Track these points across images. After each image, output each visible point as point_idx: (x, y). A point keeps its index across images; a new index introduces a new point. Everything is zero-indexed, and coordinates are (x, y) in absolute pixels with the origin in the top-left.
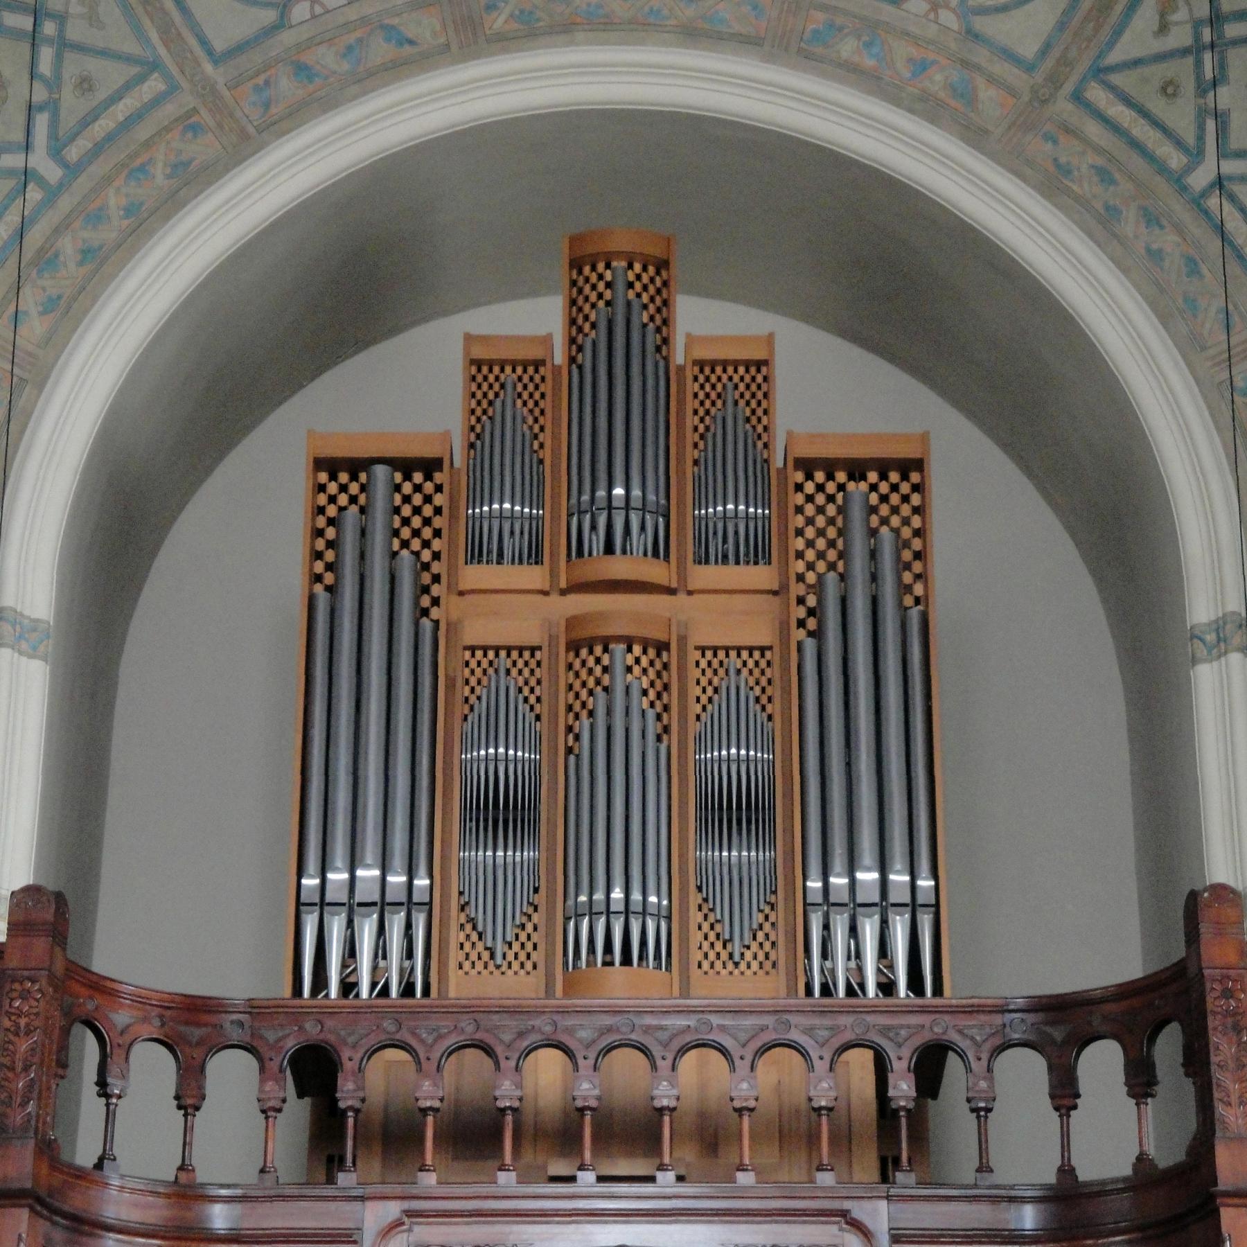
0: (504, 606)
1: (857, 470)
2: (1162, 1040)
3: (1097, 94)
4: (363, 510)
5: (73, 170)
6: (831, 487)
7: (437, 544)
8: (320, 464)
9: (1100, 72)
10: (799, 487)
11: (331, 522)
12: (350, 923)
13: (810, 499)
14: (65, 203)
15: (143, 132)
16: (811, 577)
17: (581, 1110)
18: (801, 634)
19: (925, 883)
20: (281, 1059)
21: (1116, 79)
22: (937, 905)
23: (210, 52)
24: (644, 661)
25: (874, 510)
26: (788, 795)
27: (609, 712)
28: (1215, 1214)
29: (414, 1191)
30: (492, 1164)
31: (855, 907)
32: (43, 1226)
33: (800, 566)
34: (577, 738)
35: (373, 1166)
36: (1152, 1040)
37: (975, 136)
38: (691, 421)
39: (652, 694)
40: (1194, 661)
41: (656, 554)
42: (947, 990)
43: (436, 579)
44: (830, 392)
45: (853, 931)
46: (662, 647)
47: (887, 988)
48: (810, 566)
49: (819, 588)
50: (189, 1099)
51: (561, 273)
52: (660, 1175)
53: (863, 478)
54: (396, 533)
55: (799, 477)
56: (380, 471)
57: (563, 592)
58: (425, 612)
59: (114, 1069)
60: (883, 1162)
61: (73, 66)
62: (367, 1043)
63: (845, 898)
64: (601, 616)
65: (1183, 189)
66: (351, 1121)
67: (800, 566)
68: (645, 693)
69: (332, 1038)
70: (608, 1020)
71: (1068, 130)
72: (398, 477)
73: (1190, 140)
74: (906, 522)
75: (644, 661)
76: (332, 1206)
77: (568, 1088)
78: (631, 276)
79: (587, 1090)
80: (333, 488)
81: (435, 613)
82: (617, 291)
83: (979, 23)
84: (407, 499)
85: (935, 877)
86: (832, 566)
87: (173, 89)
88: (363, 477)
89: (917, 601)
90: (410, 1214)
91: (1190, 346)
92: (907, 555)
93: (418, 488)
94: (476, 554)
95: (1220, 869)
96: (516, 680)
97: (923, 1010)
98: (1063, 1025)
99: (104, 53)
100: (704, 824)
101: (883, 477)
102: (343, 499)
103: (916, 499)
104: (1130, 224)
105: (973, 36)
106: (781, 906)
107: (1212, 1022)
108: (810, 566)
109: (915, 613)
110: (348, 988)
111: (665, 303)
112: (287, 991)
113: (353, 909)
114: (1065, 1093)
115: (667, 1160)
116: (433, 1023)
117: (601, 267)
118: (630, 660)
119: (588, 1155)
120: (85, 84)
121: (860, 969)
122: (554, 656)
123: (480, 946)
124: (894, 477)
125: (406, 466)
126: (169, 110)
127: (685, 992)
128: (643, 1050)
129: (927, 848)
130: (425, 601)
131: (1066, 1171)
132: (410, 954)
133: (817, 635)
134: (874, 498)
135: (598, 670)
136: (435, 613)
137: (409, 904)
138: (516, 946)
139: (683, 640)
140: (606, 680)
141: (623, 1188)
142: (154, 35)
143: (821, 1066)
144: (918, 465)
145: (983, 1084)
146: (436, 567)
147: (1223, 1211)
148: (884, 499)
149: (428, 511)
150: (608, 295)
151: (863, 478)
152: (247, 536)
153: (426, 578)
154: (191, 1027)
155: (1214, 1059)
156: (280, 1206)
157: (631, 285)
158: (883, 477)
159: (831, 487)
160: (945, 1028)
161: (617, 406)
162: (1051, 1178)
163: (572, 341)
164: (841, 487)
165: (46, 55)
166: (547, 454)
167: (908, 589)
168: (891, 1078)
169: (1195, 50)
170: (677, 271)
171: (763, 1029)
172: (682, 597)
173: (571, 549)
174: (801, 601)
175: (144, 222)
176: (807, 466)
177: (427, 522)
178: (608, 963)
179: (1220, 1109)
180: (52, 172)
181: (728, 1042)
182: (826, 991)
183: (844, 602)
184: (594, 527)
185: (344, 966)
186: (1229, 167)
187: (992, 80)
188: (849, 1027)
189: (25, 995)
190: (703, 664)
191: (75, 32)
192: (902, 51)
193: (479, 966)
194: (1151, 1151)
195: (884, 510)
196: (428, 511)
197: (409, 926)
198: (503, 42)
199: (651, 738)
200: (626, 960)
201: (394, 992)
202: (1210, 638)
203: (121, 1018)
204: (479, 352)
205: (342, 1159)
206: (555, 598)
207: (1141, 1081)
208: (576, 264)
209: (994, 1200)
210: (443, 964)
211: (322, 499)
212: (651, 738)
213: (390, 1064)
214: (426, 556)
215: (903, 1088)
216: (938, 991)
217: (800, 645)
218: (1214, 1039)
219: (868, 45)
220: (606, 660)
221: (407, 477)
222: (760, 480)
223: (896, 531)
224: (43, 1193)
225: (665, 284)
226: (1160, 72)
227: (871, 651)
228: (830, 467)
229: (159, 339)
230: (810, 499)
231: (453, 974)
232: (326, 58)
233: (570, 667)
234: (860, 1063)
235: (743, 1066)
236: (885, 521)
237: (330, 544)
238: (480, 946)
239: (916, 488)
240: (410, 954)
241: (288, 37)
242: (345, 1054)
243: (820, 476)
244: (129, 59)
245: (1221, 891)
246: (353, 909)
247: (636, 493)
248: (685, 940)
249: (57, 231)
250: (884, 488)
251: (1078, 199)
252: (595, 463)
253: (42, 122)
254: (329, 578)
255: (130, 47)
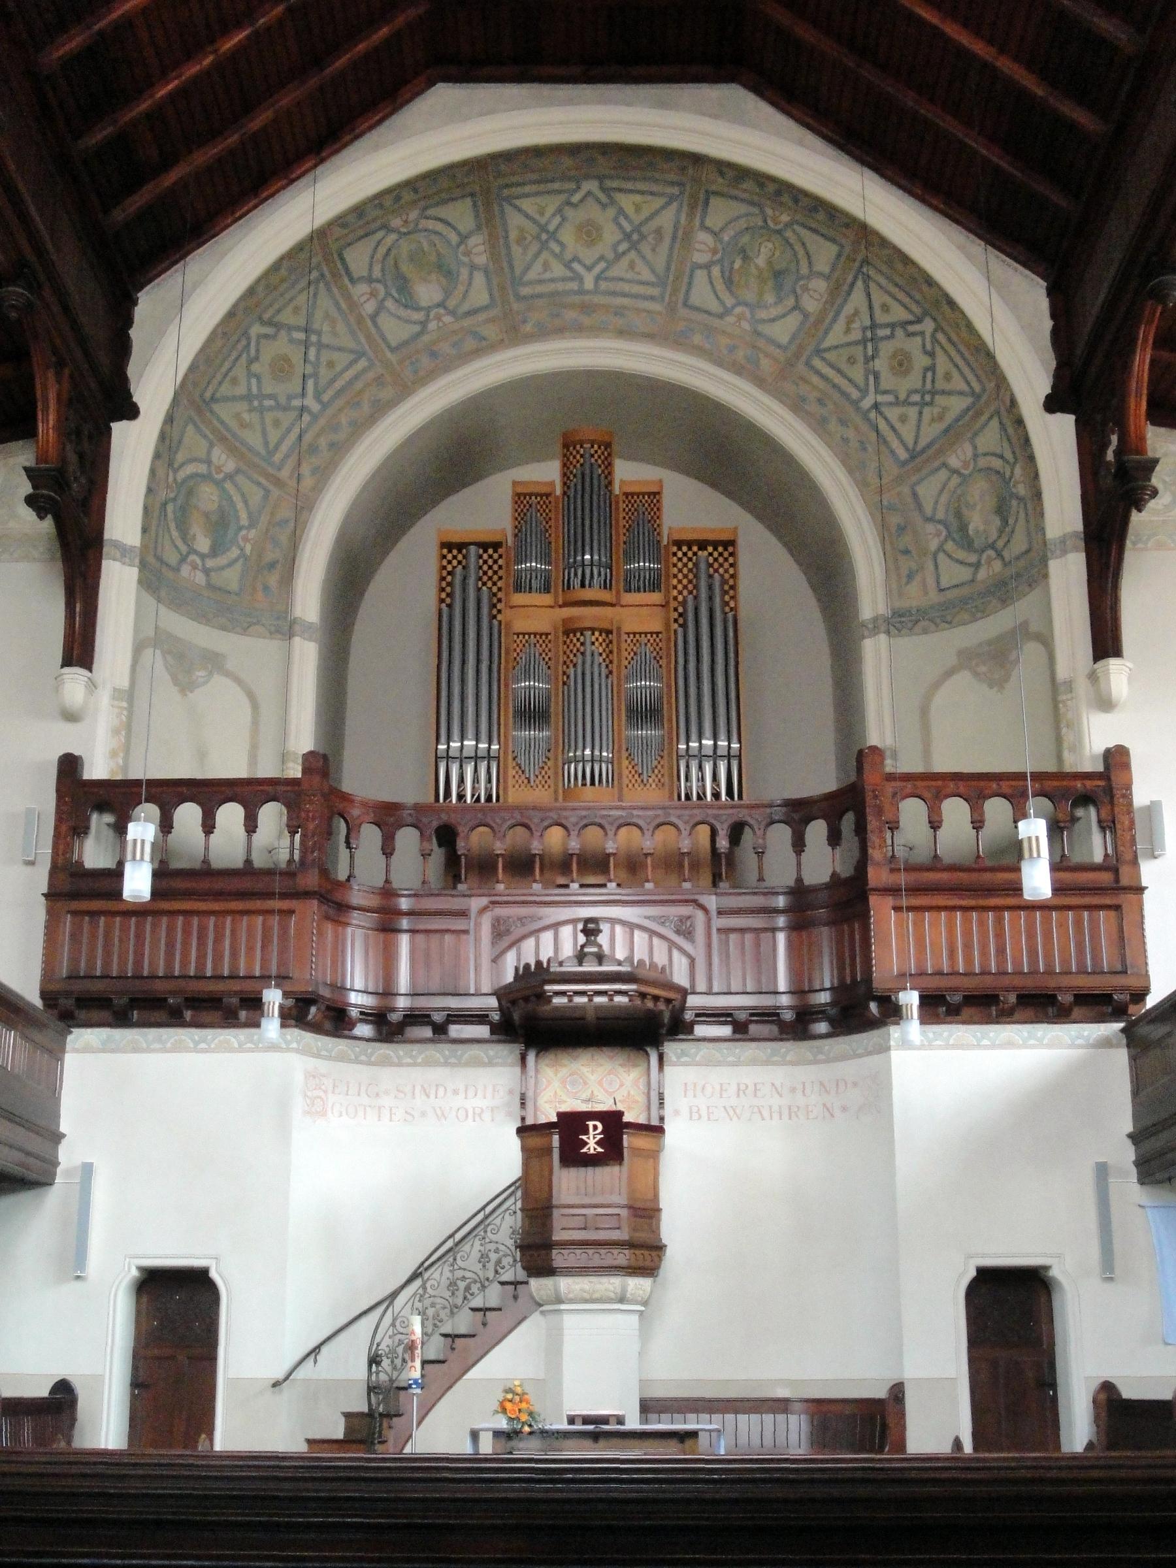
0: (533, 613)
1: (703, 545)
2: (845, 817)
3: (817, 363)
4: (464, 567)
5: (325, 406)
6: (690, 554)
7: (499, 584)
8: (444, 545)
9: (818, 352)
10: (675, 554)
11: (449, 573)
12: (461, 766)
13: (680, 559)
14: (322, 421)
15: (359, 385)
16: (680, 598)
17: (572, 855)
18: (676, 626)
19: (735, 746)
20: (430, 831)
21: (827, 355)
22: (740, 756)
23: (389, 347)
24: (600, 640)
25: (711, 565)
26: (669, 703)
27: (584, 663)
28: (866, 900)
29: (494, 892)
30: (530, 879)
31: (701, 757)
32: (325, 907)
33: (675, 593)
34: (568, 677)
35: (473, 881)
36: (840, 818)
37: (760, 382)
38: (622, 522)
39: (604, 656)
40: (864, 637)
41: (605, 588)
42: (744, 796)
43: (500, 600)
44: (690, 507)
45: (700, 768)
46: (609, 632)
47: (716, 795)
48: (680, 593)
49: (684, 603)
50: (388, 850)
51: (558, 448)
52: (609, 885)
53: (706, 549)
54: (480, 579)
55: (675, 549)
56: (473, 548)
57: (560, 606)
58: (495, 617)
59: (353, 835)
60: (714, 876)
61: (326, 356)
62: (471, 824)
63: (696, 753)
64: (579, 618)
65: (858, 409)
66: (463, 860)
67: (675, 593)
68: (601, 654)
69: (453, 821)
70: (584, 813)
71: (802, 378)
72: (481, 551)
73: (862, 385)
74: (726, 571)
75: (600, 640)
76: (455, 899)
77: (565, 844)
78: (592, 451)
79: (574, 845)
80: (450, 557)
81: (499, 617)
82: (587, 460)
83: (760, 328)
84: (485, 562)
85: (740, 742)
86: (690, 593)
87: (371, 366)
88: (464, 551)
89: (732, 609)
90: (493, 903)
91: (862, 485)
92: (726, 587)
93: (490, 557)
94: (518, 588)
95: (873, 739)
96: (539, 649)
97: (733, 807)
98: (799, 813)
99: (340, 349)
100: (629, 718)
101: (715, 549)
102: (455, 562)
103: (731, 560)
104: (833, 425)
105: (758, 333)
106: (666, 757)
107: (868, 810)
108: (680, 593)
109: (730, 615)
110: (461, 797)
111: (610, 464)
112: (432, 799)
113: (462, 760)
114: (799, 844)
115: (612, 877)
116: (502, 814)
117: (578, 447)
118: (593, 639)
119: (575, 874)
120: (331, 364)
121: (704, 787)
122: (557, 637)
123: (523, 777)
124: (720, 549)
125: (485, 546)
126: (371, 375)
127: (620, 800)
128: (601, 826)
129: (736, 729)
130: (495, 612)
131: (799, 880)
132: (489, 781)
133: (684, 626)
134: (711, 560)
135: (578, 644)
136: (499, 617)
137: (489, 758)
138: (540, 777)
139: (619, 629)
140: (582, 649)
141: (592, 891)
142: (363, 340)
143: (685, 833)
144: (732, 543)
145: (760, 841)
146: (500, 595)
147: (871, 898)
148: (716, 560)
149: (495, 567)
150: (582, 460)
151: (706, 549)
152: (409, 581)
153: (495, 600)
154: (388, 817)
155: (869, 827)
156: (432, 899)
157: (592, 456)
158: (715, 549)
159: (690, 554)
160: (743, 815)
161: (586, 518)
162: (791, 883)
163: (565, 484)
164: (695, 554)
165: (312, 352)
166: (553, 539)
167: (727, 604)
168: (718, 839)
169: (864, 342)
170: (615, 447)
171: (657, 816)
172: (618, 609)
173: (563, 587)
174: (676, 610)
175: (359, 428)
176: (679, 544)
177: (495, 573)
178: (584, 785)
179: (870, 851)
180: (315, 407)
181: (641, 823)
182: (688, 797)
183: (697, 610)
184: (576, 575)
185: (459, 787)
186: (880, 398)
187: (767, 355)
188: (699, 814)
189: (311, 802)
190: (629, 641)
191: (325, 340)
192: (724, 341)
193: (523, 787)
194: (838, 870)
195: (716, 565)
196: (495, 567)
197: (489, 768)
198: (529, 338)
199: (603, 676)
200: (593, 783)
201: (483, 799)
202: (870, 626)
203: (356, 812)
204: (519, 490)
205: (460, 876)
206: (557, 610)
207: (834, 838)
208: (566, 446)
209: (765, 894)
210: (505, 789)
211: (445, 562)
212: (603, 676)
213: (481, 833)
214: (495, 589)
215: (723, 843)
216: (740, 797)
217: (675, 631)
218: (869, 818)
219: (707, 337)
220: (582, 639)
221: (485, 551)
222: (655, 550)
223: (722, 576)
224: (323, 891)
225: (609, 455)
226: (845, 353)
227: (708, 630)
228: (690, 544)
229: (365, 487)
230: (680, 559)
231: (511, 791)
232: (445, 348)
233: (565, 643)
234: (704, 831)
235: (648, 834)
236: (716, 571)
237: (449, 584)
238: (523, 777)
239: (731, 554)
240: (489, 781)
241: (426, 338)
242: (460, 829)
243: (685, 549)
244: (351, 351)
245: (874, 749)
246: (462, 760)
247: (596, 557)
248: (620, 775)
249: (318, 435)
250: (716, 554)
251: (807, 413)
252: (578, 543)
253: (310, 383)
254: (448, 601)
255: (352, 345)
